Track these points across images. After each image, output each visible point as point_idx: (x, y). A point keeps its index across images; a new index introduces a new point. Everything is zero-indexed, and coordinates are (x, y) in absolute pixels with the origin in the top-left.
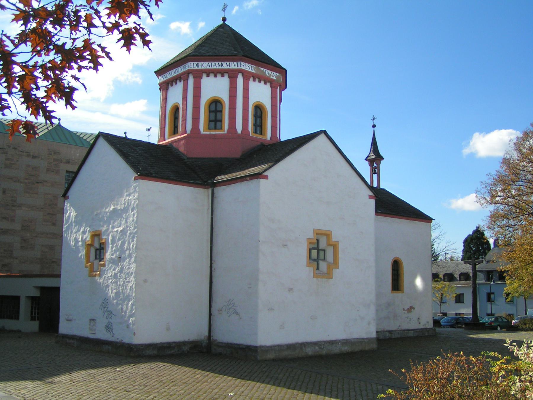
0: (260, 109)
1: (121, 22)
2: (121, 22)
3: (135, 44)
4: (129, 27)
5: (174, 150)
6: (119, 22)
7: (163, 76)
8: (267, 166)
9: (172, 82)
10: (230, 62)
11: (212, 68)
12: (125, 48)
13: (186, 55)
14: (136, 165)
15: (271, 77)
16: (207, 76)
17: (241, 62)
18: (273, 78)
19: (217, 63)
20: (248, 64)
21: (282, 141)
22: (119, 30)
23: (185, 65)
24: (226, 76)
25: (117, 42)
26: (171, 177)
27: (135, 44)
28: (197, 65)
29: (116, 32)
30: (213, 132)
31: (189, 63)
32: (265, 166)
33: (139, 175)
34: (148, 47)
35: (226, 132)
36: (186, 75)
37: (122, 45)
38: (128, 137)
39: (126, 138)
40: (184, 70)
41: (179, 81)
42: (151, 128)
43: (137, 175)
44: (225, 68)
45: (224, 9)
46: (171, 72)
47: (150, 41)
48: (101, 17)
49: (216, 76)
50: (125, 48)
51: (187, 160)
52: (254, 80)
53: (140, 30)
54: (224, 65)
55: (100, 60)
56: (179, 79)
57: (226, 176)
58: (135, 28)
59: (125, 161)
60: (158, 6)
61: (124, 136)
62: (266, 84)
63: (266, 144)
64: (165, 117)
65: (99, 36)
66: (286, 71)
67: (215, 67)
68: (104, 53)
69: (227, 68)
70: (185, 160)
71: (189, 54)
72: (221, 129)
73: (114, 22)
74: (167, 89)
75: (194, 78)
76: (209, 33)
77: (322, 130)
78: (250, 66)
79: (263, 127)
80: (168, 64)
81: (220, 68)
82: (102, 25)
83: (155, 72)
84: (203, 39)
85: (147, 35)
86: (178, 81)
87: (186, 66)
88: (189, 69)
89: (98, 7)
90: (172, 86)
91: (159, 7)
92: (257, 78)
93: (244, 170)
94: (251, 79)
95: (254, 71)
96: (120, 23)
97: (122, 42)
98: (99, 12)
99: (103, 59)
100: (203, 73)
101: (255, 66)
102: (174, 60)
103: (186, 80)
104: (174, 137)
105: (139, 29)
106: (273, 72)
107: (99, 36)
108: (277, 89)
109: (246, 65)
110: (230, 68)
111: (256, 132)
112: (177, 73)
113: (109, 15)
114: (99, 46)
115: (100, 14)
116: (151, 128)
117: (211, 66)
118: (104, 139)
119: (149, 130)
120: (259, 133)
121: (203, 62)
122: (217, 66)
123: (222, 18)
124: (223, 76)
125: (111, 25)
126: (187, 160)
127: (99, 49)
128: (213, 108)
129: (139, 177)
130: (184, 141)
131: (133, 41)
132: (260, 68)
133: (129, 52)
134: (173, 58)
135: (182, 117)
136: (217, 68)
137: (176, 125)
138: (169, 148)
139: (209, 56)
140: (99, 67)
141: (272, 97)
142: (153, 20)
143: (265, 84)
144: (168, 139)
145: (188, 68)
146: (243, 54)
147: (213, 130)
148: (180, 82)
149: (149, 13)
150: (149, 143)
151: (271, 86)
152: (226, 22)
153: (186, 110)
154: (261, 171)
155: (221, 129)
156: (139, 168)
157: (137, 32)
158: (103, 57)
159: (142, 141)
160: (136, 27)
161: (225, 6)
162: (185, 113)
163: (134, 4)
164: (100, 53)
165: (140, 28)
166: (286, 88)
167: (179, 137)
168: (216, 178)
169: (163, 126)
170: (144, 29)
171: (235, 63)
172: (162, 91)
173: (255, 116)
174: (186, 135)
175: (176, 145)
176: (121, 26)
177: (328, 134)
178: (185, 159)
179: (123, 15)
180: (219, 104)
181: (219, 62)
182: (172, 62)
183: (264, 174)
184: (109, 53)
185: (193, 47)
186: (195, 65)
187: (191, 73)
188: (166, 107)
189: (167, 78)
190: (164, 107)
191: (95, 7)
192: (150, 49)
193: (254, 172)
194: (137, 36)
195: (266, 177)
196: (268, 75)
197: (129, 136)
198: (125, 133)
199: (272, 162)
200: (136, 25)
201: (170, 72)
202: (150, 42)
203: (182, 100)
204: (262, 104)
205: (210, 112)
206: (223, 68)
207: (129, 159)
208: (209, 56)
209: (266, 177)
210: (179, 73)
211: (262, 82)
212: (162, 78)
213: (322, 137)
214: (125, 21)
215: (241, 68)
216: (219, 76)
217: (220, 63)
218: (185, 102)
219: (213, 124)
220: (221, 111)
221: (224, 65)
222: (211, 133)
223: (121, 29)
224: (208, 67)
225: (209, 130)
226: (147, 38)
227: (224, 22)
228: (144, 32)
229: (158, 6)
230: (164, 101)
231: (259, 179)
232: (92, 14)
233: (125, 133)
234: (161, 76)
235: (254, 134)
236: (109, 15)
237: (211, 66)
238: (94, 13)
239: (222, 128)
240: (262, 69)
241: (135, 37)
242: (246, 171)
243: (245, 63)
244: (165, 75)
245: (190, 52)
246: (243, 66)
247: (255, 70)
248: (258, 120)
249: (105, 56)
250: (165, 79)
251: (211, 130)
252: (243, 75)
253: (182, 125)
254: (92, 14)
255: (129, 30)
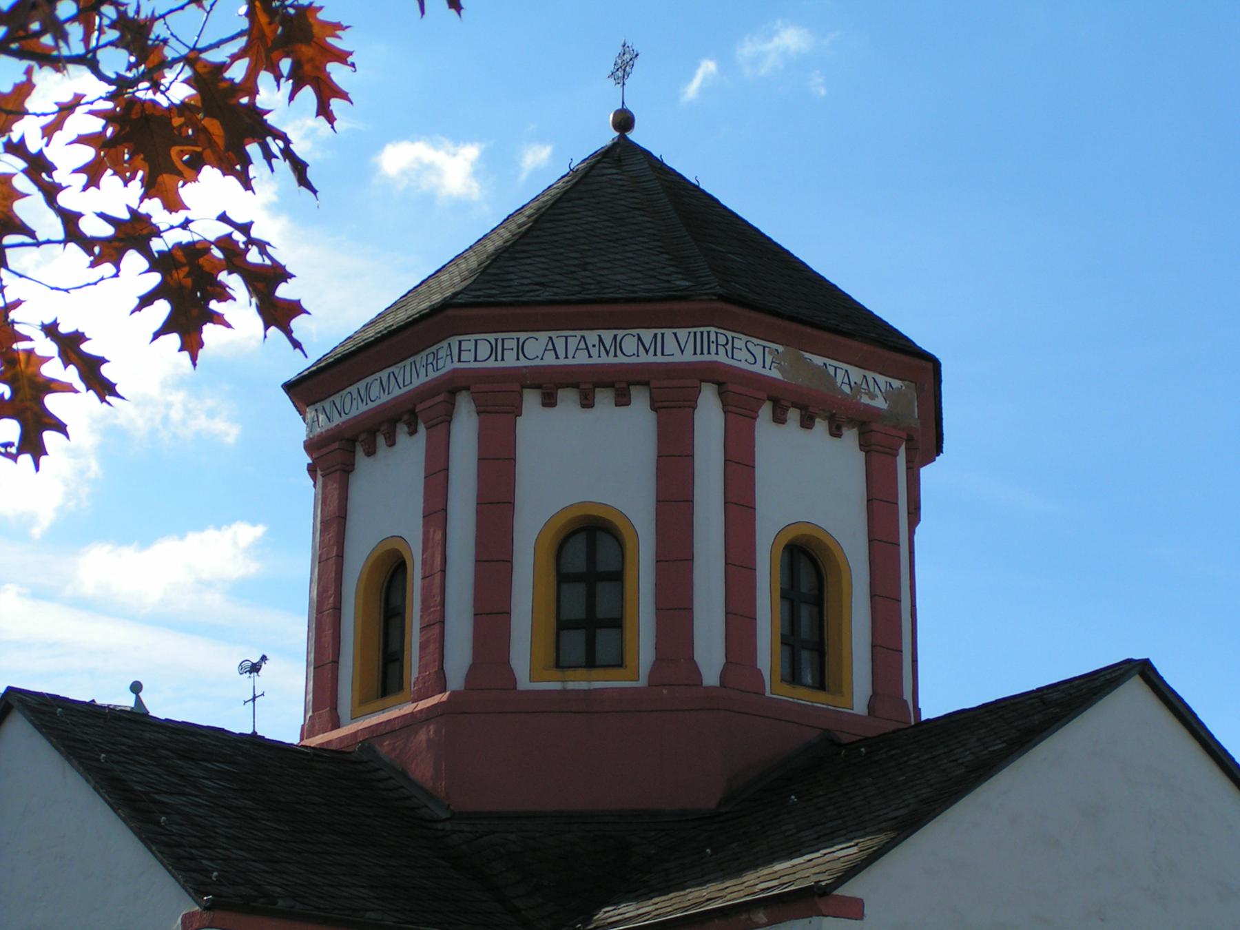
0: (814, 562)
1: (154, 208)
2: (154, 208)
3: (218, 319)
4: (196, 238)
5: (382, 774)
6: (149, 217)
7: (327, 404)
8: (855, 850)
9: (372, 433)
10: (659, 331)
11: (570, 361)
12: (174, 339)
13: (437, 298)
14: (193, 858)
15: (865, 400)
16: (545, 405)
17: (713, 330)
18: (873, 403)
19: (592, 336)
20: (745, 338)
21: (928, 721)
22: (146, 252)
23: (434, 349)
24: (640, 401)
25: (139, 308)
26: (368, 915)
27: (218, 319)
28: (493, 350)
29: (133, 261)
30: (580, 683)
31: (454, 341)
32: (845, 852)
33: (207, 909)
34: (288, 333)
35: (642, 682)
36: (440, 398)
37: (158, 325)
38: (154, 712)
39: (138, 718)
40: (432, 375)
41: (406, 429)
42: (264, 658)
43: (197, 908)
44: (634, 360)
45: (622, 70)
46: (368, 388)
47: (299, 302)
48: (59, 188)
49: (587, 402)
50: (174, 339)
51: (448, 826)
52: (779, 418)
53: (247, 250)
54: (630, 345)
55: (53, 403)
56: (406, 417)
57: (647, 907)
58: (225, 243)
59: (138, 834)
60: (331, 119)
61: (128, 701)
62: (839, 436)
63: (845, 739)
64: (338, 608)
65: (52, 288)
66: (935, 364)
67: (582, 359)
68: (72, 369)
69: (644, 358)
70: (440, 826)
71: (455, 295)
72: (620, 664)
73: (125, 215)
74: (347, 469)
75: (479, 413)
76: (553, 192)
77: (1129, 661)
78: (757, 346)
79: (830, 649)
80: (350, 346)
81: (611, 360)
82: (59, 233)
83: (289, 387)
84: (521, 219)
85: (279, 274)
86: (402, 430)
87: (442, 353)
88: (455, 370)
89: (47, 145)
90: (371, 452)
91: (336, 124)
92: (795, 405)
93: (738, 872)
94: (766, 411)
95: (775, 374)
96: (154, 221)
97: (162, 309)
98: (50, 168)
99: (71, 394)
100: (523, 387)
101: (781, 348)
102: (381, 327)
103: (442, 423)
104: (383, 710)
105: (242, 246)
106: (870, 375)
107: (52, 288)
108: (896, 455)
109: (738, 343)
110: (660, 359)
111: (793, 677)
112: (397, 392)
113: (93, 173)
114: (51, 330)
115: (50, 176)
116: (264, 658)
117: (561, 353)
118: (31, 722)
119: (255, 668)
120: (808, 679)
121: (523, 336)
122: (594, 352)
123: (611, 116)
124: (623, 399)
125: (108, 231)
126: (448, 826)
127: (45, 347)
128: (576, 561)
129: (206, 915)
130: (432, 728)
131: (214, 305)
132: (807, 355)
133: (194, 359)
134: (373, 315)
135: (425, 607)
136: (595, 360)
137: (394, 646)
138: (360, 763)
139: (552, 303)
140: (50, 437)
141: (869, 501)
142: (315, 192)
143: (832, 434)
144: (354, 718)
145: (449, 366)
146: (720, 291)
147: (582, 672)
148: (413, 432)
149: (218, 47)
150: (254, 739)
151: (865, 446)
152: (633, 136)
153: (443, 571)
154: (825, 880)
155: (620, 664)
156: (206, 872)
157: (234, 258)
158: (69, 388)
159: (222, 730)
160: (230, 235)
161: (627, 57)
162: (436, 590)
163: (224, 126)
164: (54, 369)
165: (251, 241)
166: (939, 450)
167: (408, 708)
168: (600, 915)
169: (328, 657)
170: (269, 249)
171: (683, 333)
172: (320, 480)
173: (790, 595)
174: (443, 697)
175: (394, 749)
176: (157, 233)
177: (1161, 678)
178: (436, 821)
179: (166, 178)
180: (605, 544)
181: (603, 333)
182: (371, 334)
183: (841, 891)
184: (103, 361)
185: (473, 262)
186: (484, 350)
187: (468, 389)
188: (340, 556)
189: (345, 418)
190: (332, 561)
191: (34, 146)
192: (297, 345)
193: (791, 883)
194: (234, 282)
195: (854, 909)
196: (846, 389)
197: (159, 708)
198: (136, 688)
199: (881, 831)
200: (226, 229)
201: (361, 385)
202: (295, 308)
203: (420, 521)
204: (822, 537)
205: (563, 578)
206: (621, 359)
207: (158, 823)
208: (552, 303)
209: (854, 909)
210: (404, 390)
211: (821, 426)
212: (322, 417)
213: (1134, 691)
214: (173, 204)
215: (713, 358)
216: (604, 398)
217: (607, 335)
218: (439, 535)
219: (575, 641)
220: (617, 577)
221: (630, 345)
222: (571, 686)
223: (157, 245)
224: (550, 359)
225: (558, 673)
226: (284, 291)
227: (623, 137)
228: (268, 262)
229: (331, 119)
230: (333, 529)
231: (816, 919)
232: (14, 175)
233: (136, 688)
234: (318, 406)
235: (787, 688)
236: (93, 173)
237: (561, 353)
238: (25, 171)
239: (622, 663)
240: (818, 360)
241: (223, 287)
242: (750, 878)
243: (730, 334)
244: (337, 398)
245: (458, 288)
246: (721, 349)
247: (780, 369)
248: (805, 612)
249: (79, 385)
250: (337, 420)
251: (570, 673)
252: (722, 394)
253: (423, 646)
254: (14, 175)
255: (194, 251)
